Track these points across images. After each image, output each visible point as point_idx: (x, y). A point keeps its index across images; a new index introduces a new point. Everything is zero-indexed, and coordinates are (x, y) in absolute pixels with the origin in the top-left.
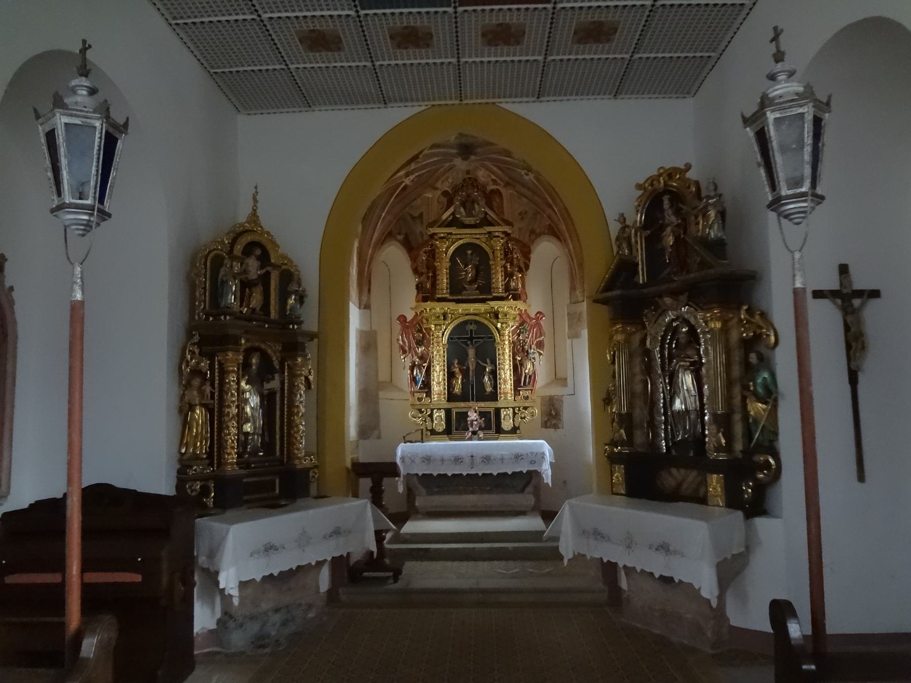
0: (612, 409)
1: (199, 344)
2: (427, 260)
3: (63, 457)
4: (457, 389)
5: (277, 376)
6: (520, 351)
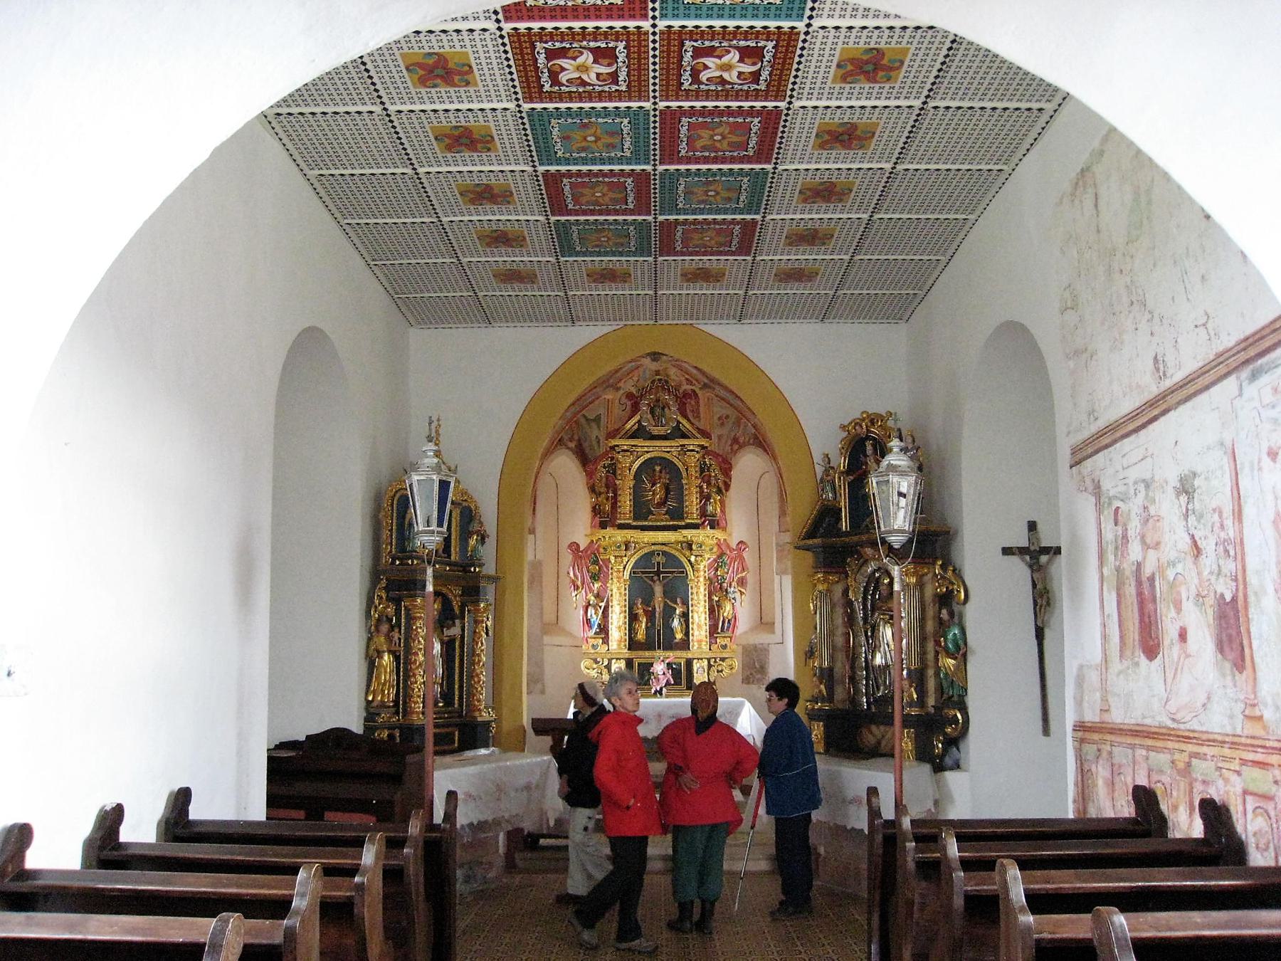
0: (814, 663)
1: (387, 589)
2: (607, 478)
4: (641, 635)
5: (457, 622)
6: (717, 590)
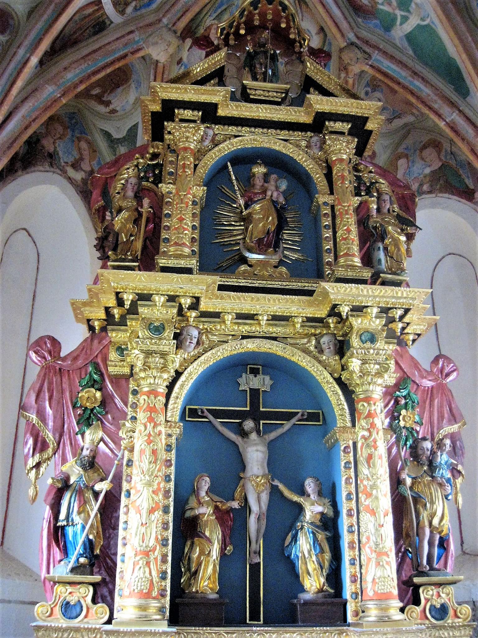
3: (4, 515)
